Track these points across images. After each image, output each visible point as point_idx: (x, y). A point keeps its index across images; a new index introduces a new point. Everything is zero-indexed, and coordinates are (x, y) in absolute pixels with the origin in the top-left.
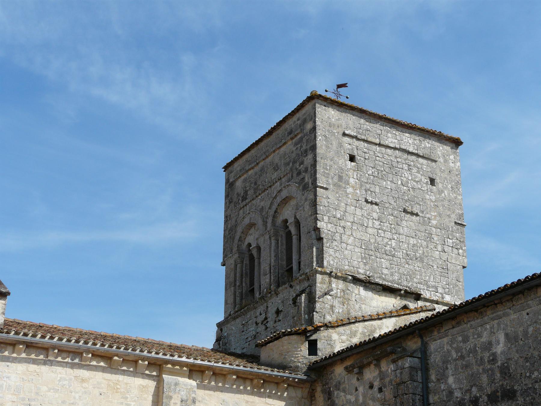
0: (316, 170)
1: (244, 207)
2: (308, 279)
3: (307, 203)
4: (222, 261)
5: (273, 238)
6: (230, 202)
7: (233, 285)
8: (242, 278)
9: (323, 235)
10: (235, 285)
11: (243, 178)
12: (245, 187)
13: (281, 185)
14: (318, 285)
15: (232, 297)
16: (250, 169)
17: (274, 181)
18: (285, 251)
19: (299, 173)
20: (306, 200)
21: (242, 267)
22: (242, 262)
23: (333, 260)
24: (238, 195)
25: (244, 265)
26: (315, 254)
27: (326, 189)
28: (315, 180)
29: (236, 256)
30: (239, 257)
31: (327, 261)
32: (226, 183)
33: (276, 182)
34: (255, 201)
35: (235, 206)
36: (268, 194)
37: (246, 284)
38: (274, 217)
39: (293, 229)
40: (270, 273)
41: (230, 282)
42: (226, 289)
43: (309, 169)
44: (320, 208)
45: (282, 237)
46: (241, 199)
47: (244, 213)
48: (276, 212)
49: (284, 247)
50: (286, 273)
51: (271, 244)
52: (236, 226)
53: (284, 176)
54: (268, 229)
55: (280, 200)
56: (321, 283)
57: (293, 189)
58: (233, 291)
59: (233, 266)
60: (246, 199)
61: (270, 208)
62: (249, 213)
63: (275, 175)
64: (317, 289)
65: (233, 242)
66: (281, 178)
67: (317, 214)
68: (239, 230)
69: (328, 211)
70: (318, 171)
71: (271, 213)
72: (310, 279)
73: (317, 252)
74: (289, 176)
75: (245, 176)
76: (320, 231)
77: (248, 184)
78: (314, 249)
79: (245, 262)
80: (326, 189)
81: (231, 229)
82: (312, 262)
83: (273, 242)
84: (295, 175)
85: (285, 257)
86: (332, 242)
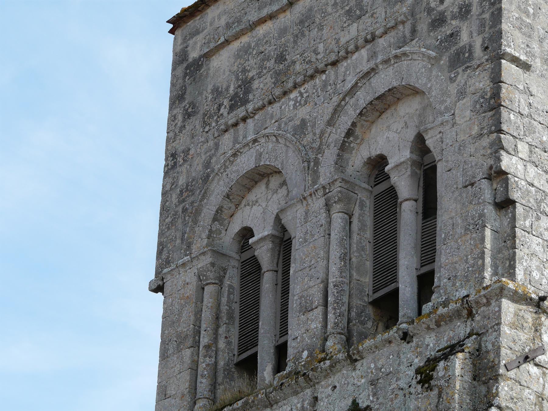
0: (500, 10)
1: (236, 125)
2: (470, 315)
3: (467, 101)
4: (152, 277)
5: (337, 207)
6: (188, 115)
7: (190, 342)
8: (218, 327)
9: (515, 195)
10: (196, 344)
11: (236, 45)
12: (244, 71)
13: (373, 55)
14: (505, 329)
15: (186, 376)
16: (262, 21)
17: (351, 47)
18: (369, 248)
19: (439, 21)
20: (462, 94)
21: (219, 294)
22: (220, 281)
23: (538, 268)
24: (217, 92)
25: (226, 289)
26: (488, 244)
27: (526, 67)
28: (497, 36)
29: (207, 260)
30: (213, 264)
31: (525, 270)
32: (176, 65)
33: (357, 48)
34: (276, 106)
35: (205, 124)
36: (325, 84)
37: (229, 343)
38: (344, 147)
39: (404, 185)
40: (326, 304)
41: (178, 336)
42: (164, 356)
43: (475, 10)
44: (510, 119)
45: (362, 205)
46: (226, 102)
47: (236, 141)
48: (349, 133)
49: (369, 234)
50: (370, 310)
51: (330, 223)
52: (206, 179)
53: (385, 33)
54: (322, 181)
55: (369, 98)
56: (513, 326)
57: (419, 68)
58: (187, 360)
59: (191, 291)
60: (245, 102)
61: (330, 123)
62: (255, 141)
63: (354, 31)
64: (504, 342)
65: (195, 222)
66: (373, 39)
67: (500, 131)
68: (218, 189)
69: (530, 130)
70: (505, 13)
71: (334, 137)
72: (476, 309)
73: (495, 239)
74: (407, 29)
75: (245, 39)
76: (507, 180)
77: (252, 62)
78: (488, 233)
79: (227, 282)
80: (526, 67)
81: (189, 189)
82: (482, 268)
83: (338, 219)
84: (423, 27)
85: (369, 265)
86: (538, 218)
